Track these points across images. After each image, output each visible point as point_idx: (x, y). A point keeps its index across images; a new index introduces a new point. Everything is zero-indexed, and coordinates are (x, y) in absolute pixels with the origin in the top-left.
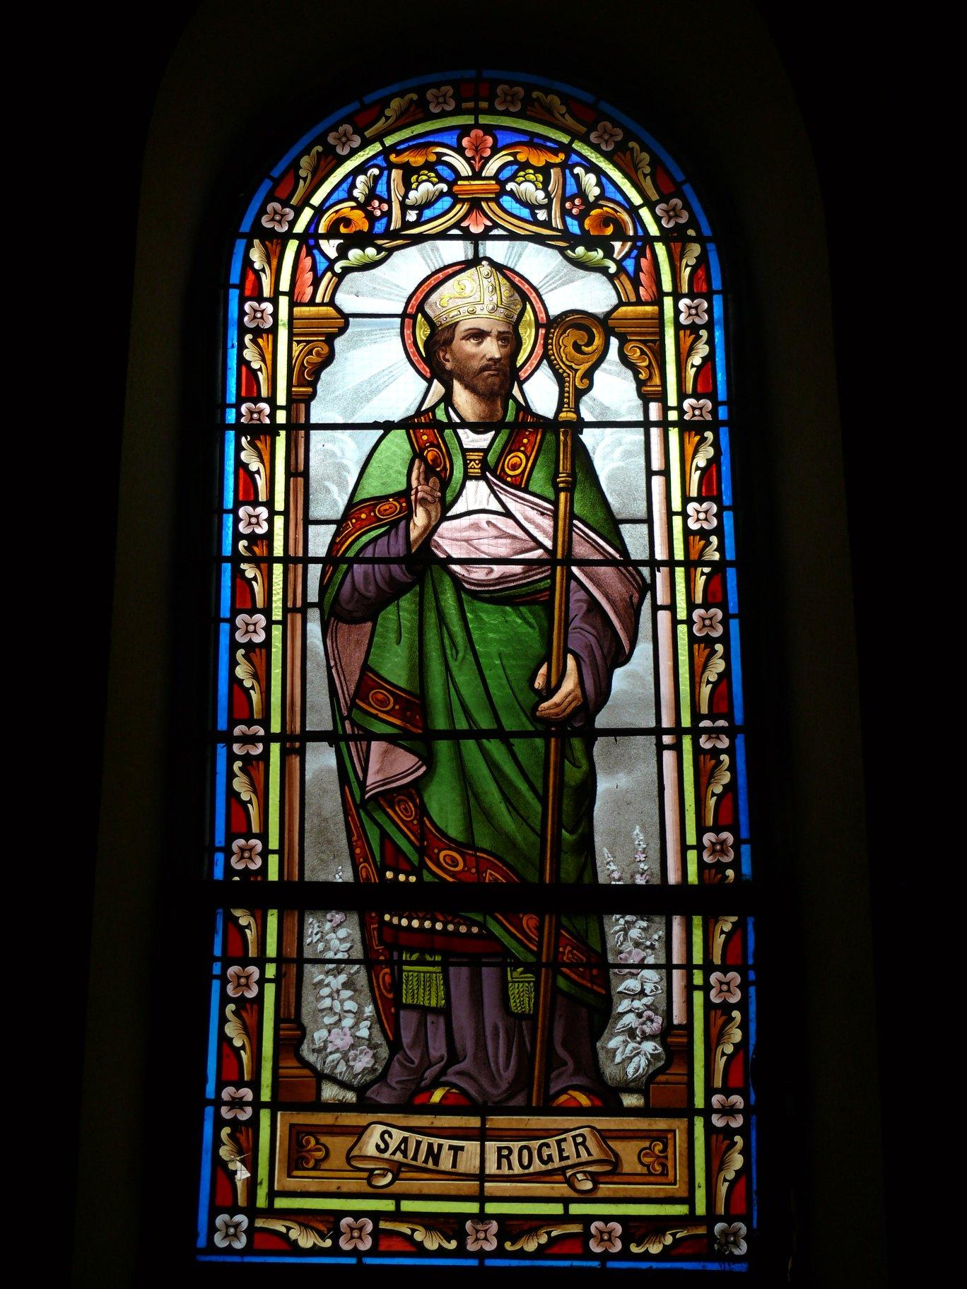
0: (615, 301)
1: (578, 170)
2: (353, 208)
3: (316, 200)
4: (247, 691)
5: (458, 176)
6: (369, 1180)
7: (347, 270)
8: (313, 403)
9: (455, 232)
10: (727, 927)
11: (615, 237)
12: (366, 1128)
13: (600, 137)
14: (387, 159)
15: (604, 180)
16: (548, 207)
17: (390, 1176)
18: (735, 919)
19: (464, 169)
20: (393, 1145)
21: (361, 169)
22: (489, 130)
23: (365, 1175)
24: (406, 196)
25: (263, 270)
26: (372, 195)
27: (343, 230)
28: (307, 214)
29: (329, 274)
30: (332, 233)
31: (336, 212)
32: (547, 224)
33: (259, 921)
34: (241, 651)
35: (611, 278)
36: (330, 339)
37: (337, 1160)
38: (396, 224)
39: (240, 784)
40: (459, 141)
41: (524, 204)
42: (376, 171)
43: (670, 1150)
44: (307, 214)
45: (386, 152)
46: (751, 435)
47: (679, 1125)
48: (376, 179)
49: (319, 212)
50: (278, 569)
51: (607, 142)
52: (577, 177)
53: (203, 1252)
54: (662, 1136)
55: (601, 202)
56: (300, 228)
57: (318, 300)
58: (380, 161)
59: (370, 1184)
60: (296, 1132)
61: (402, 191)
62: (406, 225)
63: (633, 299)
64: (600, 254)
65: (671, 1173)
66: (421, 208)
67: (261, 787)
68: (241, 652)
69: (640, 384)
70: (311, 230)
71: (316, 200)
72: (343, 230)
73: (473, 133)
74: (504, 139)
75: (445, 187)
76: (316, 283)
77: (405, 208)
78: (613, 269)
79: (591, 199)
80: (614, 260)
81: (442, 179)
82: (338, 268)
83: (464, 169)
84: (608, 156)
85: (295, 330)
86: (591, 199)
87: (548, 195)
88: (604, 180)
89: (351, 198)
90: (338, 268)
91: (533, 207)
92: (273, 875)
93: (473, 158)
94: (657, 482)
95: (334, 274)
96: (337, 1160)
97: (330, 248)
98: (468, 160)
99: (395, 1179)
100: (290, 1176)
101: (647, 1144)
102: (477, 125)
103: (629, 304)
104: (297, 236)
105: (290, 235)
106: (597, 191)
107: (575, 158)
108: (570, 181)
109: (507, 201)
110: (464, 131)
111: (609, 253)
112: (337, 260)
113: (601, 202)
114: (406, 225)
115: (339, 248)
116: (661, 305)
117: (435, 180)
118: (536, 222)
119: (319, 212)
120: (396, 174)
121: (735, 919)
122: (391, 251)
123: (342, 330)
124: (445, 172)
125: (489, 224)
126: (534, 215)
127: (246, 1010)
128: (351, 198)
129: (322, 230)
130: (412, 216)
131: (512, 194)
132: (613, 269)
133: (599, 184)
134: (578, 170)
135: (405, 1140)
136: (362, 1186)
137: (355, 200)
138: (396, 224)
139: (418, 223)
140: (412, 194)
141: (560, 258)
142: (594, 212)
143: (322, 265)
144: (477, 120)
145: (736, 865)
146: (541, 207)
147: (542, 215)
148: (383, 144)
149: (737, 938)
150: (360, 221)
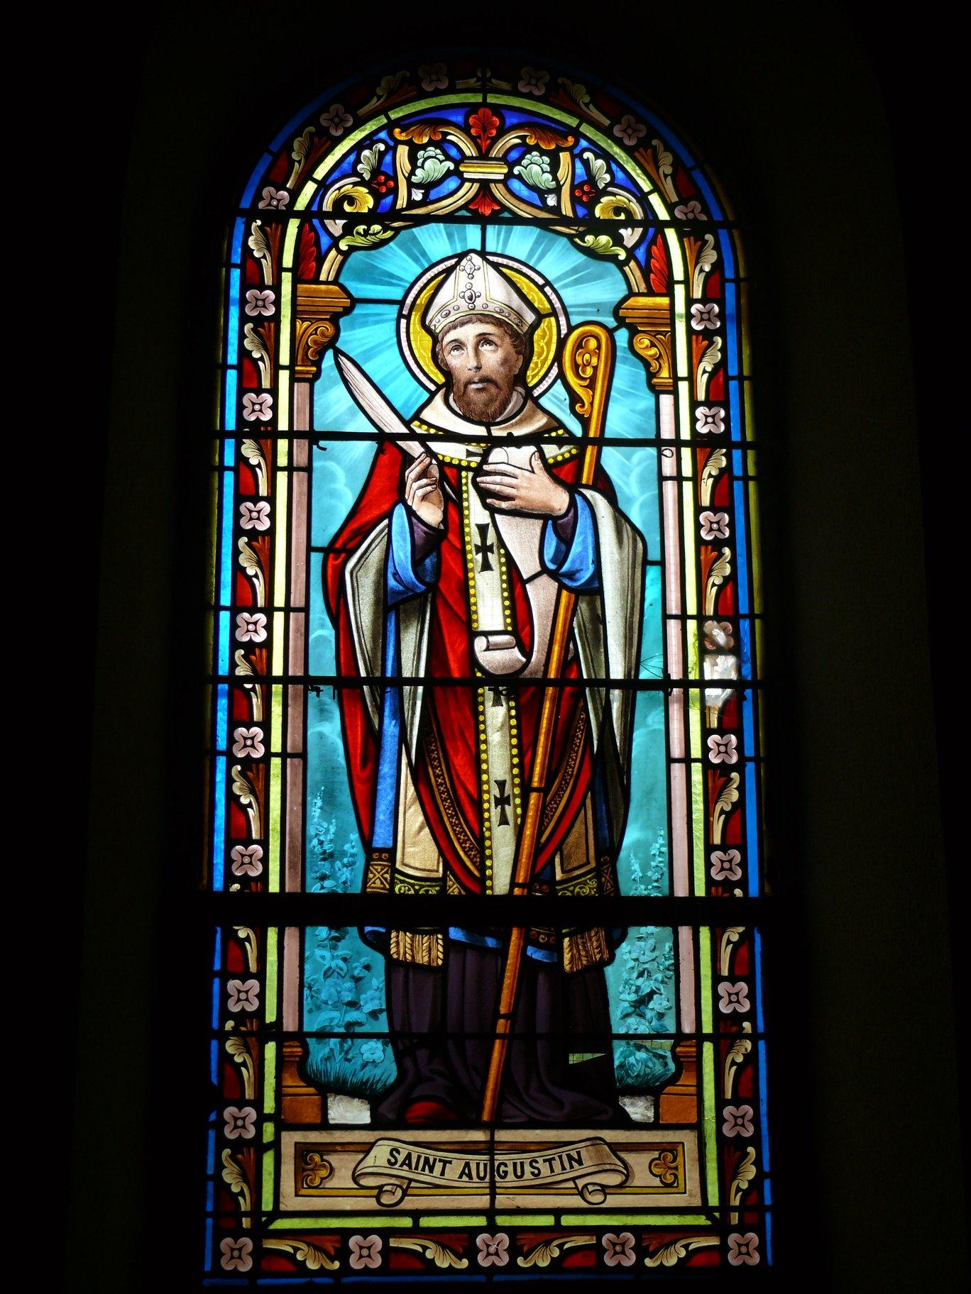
0: (623, 291)
1: (587, 155)
2: (355, 184)
3: (320, 173)
4: (249, 578)
5: (463, 158)
6: (378, 1198)
7: (352, 249)
8: (318, 384)
9: (464, 213)
10: (735, 938)
11: (625, 224)
12: (372, 1145)
13: (624, 131)
14: (391, 135)
15: (614, 167)
16: (557, 191)
17: (399, 1193)
18: (741, 929)
19: (469, 150)
20: (401, 1158)
21: (367, 142)
22: (497, 110)
23: (375, 1192)
24: (412, 173)
25: (264, 257)
26: (376, 172)
27: (347, 208)
28: (310, 188)
29: (333, 253)
30: (338, 212)
31: (339, 189)
32: (557, 209)
33: (267, 573)
34: (244, 540)
35: (621, 265)
36: (334, 319)
37: (343, 1179)
38: (402, 202)
39: (230, 1176)
40: (466, 120)
41: (533, 188)
42: (382, 147)
43: (680, 1159)
44: (310, 188)
45: (390, 127)
46: (781, 456)
47: (688, 1139)
48: (382, 155)
49: (323, 186)
50: (277, 689)
51: (630, 136)
52: (586, 163)
53: (208, 1275)
54: (672, 1148)
55: (610, 189)
56: (301, 204)
57: (323, 277)
58: (383, 135)
59: (379, 1202)
60: (302, 1151)
61: (408, 167)
62: (412, 204)
63: (643, 288)
64: (604, 239)
65: (682, 1186)
66: (428, 186)
67: (271, 343)
68: (244, 540)
69: (651, 376)
70: (315, 208)
71: (320, 173)
72: (347, 208)
73: (481, 111)
74: (511, 120)
75: (452, 166)
76: (321, 259)
77: (411, 185)
78: (622, 255)
79: (601, 185)
80: (624, 247)
81: (448, 158)
82: (343, 245)
83: (469, 150)
84: (629, 151)
85: (299, 308)
86: (601, 185)
87: (555, 178)
88: (614, 167)
89: (355, 173)
90: (343, 245)
91: (542, 193)
92: (274, 887)
93: (479, 137)
94: (670, 488)
95: (339, 251)
96: (343, 1179)
97: (336, 227)
98: (474, 140)
99: (405, 1194)
100: (297, 1195)
101: (656, 1155)
102: (484, 104)
103: (640, 294)
104: (297, 214)
105: (290, 213)
106: (608, 177)
107: (584, 143)
108: (579, 165)
109: (516, 185)
110: (472, 108)
111: (618, 241)
112: (342, 237)
113: (610, 189)
114: (412, 204)
115: (344, 227)
116: (671, 296)
117: (442, 157)
118: (545, 208)
119: (323, 186)
120: (403, 151)
121: (741, 929)
122: (397, 231)
123: (348, 311)
124: (453, 152)
125: (497, 208)
126: (544, 200)
127: (251, 770)
128: (355, 173)
129: (327, 206)
130: (418, 195)
131: (519, 177)
132: (622, 255)
133: (609, 171)
134: (587, 155)
135: (409, 1156)
136: (371, 1204)
137: (360, 175)
138: (402, 202)
139: (424, 203)
140: (418, 172)
141: (569, 244)
142: (604, 200)
143: (325, 241)
144: (485, 98)
145: (743, 884)
146: (550, 191)
147: (551, 201)
148: (388, 117)
149: (744, 951)
150: (366, 202)
